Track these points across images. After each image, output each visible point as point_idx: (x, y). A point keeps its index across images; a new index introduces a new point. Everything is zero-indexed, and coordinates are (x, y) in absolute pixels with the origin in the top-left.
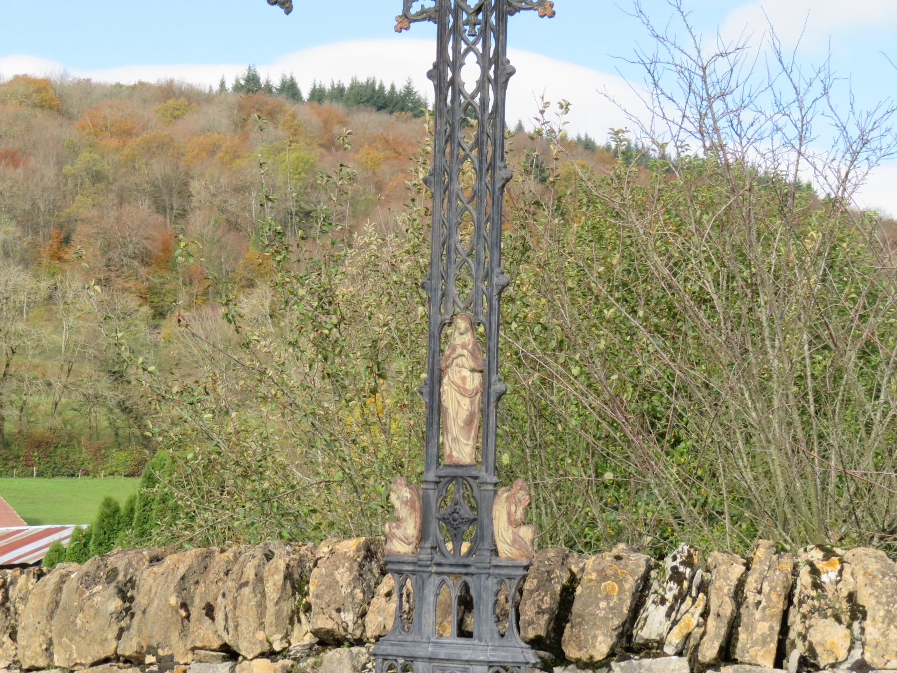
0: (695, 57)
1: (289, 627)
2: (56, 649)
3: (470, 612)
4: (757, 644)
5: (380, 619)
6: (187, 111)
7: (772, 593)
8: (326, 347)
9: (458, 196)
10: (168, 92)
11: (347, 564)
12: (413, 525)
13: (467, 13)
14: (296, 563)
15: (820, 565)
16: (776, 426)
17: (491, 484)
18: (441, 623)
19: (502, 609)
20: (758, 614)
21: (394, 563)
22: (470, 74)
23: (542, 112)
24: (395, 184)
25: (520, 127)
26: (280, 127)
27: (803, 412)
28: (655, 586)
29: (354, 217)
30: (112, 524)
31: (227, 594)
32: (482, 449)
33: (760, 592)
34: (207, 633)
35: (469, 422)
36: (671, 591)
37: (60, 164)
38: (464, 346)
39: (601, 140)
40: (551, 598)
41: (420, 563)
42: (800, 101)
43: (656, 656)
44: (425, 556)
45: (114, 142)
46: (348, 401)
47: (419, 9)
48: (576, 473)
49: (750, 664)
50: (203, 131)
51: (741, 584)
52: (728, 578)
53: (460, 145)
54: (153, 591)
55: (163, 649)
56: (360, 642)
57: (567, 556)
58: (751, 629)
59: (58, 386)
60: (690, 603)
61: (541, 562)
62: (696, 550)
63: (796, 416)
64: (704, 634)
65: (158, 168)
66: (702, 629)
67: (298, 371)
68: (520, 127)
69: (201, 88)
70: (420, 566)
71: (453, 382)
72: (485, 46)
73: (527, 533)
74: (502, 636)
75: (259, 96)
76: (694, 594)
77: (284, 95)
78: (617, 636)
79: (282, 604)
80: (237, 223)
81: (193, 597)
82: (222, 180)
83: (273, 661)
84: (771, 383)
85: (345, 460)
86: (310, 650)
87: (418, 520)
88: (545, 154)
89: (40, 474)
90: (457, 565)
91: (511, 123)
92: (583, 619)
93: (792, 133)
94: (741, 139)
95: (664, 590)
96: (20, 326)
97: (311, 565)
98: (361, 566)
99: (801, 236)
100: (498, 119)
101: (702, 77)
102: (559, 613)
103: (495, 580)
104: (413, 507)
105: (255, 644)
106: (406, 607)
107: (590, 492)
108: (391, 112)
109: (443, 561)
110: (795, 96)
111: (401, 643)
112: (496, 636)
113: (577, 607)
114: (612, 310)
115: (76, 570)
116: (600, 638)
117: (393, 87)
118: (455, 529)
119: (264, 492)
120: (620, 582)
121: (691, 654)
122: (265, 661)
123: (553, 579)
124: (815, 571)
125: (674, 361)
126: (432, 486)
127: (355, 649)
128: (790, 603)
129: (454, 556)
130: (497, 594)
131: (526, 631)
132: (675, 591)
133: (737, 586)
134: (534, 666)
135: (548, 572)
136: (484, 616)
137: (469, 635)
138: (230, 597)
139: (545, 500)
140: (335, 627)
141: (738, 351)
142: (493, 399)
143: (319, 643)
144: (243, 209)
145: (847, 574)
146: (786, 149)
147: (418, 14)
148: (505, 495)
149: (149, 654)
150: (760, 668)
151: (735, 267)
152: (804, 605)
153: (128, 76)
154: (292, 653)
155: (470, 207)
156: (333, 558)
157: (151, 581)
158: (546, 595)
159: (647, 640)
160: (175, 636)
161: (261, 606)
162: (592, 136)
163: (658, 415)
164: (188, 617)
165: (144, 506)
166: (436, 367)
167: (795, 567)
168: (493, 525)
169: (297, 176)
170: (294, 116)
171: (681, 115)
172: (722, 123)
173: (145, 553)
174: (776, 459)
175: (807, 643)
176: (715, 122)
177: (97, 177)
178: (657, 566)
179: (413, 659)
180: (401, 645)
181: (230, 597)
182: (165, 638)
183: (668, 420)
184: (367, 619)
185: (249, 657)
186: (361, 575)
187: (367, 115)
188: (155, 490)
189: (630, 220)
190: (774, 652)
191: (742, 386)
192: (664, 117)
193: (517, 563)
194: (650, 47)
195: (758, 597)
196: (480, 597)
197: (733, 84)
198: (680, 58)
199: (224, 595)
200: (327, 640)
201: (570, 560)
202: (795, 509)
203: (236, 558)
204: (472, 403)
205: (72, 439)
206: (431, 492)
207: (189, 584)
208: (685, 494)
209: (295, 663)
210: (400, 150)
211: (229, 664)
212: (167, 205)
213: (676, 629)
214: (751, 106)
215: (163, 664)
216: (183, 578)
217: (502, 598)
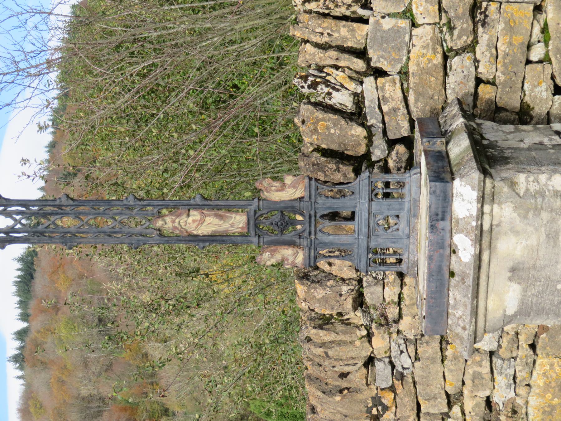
1: (352, 325)
3: (339, 213)
4: (354, 35)
5: (345, 269)
6: (37, 399)
7: (322, 26)
8: (181, 306)
9: (79, 228)
11: (312, 291)
12: (286, 250)
14: (312, 323)
16: (222, 25)
17: (259, 202)
18: (346, 231)
19: (337, 193)
20: (336, 35)
21: (310, 262)
23: (29, 177)
24: (80, 267)
25: (42, 189)
26: (45, 340)
27: (213, 8)
28: (320, 99)
29: (101, 292)
31: (333, 365)
33: (322, 34)
34: (358, 376)
35: (221, 217)
36: (322, 89)
38: (173, 222)
39: (47, 137)
40: (329, 163)
41: (309, 245)
42: (18, 14)
43: (363, 97)
44: (305, 242)
46: (214, 293)
48: (255, 149)
49: (367, 39)
51: (317, 45)
52: (314, 53)
54: (333, 411)
55: (368, 404)
56: (360, 281)
57: (303, 154)
58: (345, 39)
60: (330, 77)
61: (307, 170)
62: (297, 74)
63: (216, 13)
64: (349, 68)
66: (346, 69)
67: (195, 323)
68: (42, 189)
69: (22, 391)
70: (311, 245)
71: (196, 228)
73: (289, 179)
74: (353, 193)
75: (26, 353)
76: (324, 75)
77: (25, 339)
78: (351, 122)
79: (338, 330)
80: (107, 365)
81: (336, 386)
82: (80, 376)
83: (373, 335)
84: (196, 29)
85: (251, 293)
86: (366, 312)
87: (283, 247)
88: (60, 172)
90: (310, 222)
91: (37, 195)
92: (342, 143)
95: (322, 93)
97: (313, 313)
98: (313, 282)
100: (30, 204)
101: (4, 75)
102: (338, 158)
103: (319, 198)
104: (275, 251)
105: (363, 347)
106: (337, 253)
107: (267, 140)
108: (35, 270)
109: (308, 231)
110: (14, 17)
111: (359, 255)
112: (353, 197)
113: (334, 147)
114: (153, 130)
116: (353, 132)
117: (19, 270)
118: (288, 224)
119: (272, 342)
120: (318, 120)
121: (361, 76)
122: (374, 339)
123: (317, 162)
125: (184, 90)
126: (261, 239)
127: (365, 284)
128: (328, 15)
129: (304, 224)
130: (327, 197)
131: (350, 178)
132: (323, 86)
133: (319, 48)
134: (371, 173)
135: (313, 165)
136: (341, 205)
137: (353, 213)
138: (335, 363)
139: (273, 168)
140: (351, 297)
141: (176, 50)
142: (206, 203)
143: (361, 307)
144: (98, 362)
146: (49, 23)
148: (265, 193)
149: (371, 412)
150: (369, 33)
151: (124, 53)
152: (330, 6)
154: (368, 323)
155: (85, 220)
156: (309, 299)
157: (326, 412)
158: (328, 167)
159: (353, 103)
160: (360, 396)
161: (340, 343)
163: (218, 99)
164: (348, 389)
165: (285, 417)
166: (187, 239)
168: (284, 201)
169: (77, 329)
170: (38, 332)
171: (28, 88)
172: (33, 63)
173: (309, 417)
174: (244, 25)
175: (353, 4)
176: (32, 67)
178: (308, 98)
179: (369, 248)
180: (361, 256)
181: (335, 363)
182: (361, 402)
183: (221, 93)
184: (346, 277)
185: (371, 350)
186: (318, 282)
187: (36, 286)
188: (274, 411)
189: (96, 119)
190: (359, 24)
191: (198, 47)
192: (30, 99)
193: (307, 185)
195: (325, 35)
196: (329, 208)
197: (9, 56)
199: (334, 367)
200: (359, 302)
201: (306, 152)
203: (311, 360)
204: (209, 216)
206: (265, 240)
208: (266, 81)
209: (374, 321)
210: (58, 264)
211: (376, 362)
212: (97, 410)
213: (346, 85)
215: (377, 403)
216: (324, 393)
217: (330, 194)
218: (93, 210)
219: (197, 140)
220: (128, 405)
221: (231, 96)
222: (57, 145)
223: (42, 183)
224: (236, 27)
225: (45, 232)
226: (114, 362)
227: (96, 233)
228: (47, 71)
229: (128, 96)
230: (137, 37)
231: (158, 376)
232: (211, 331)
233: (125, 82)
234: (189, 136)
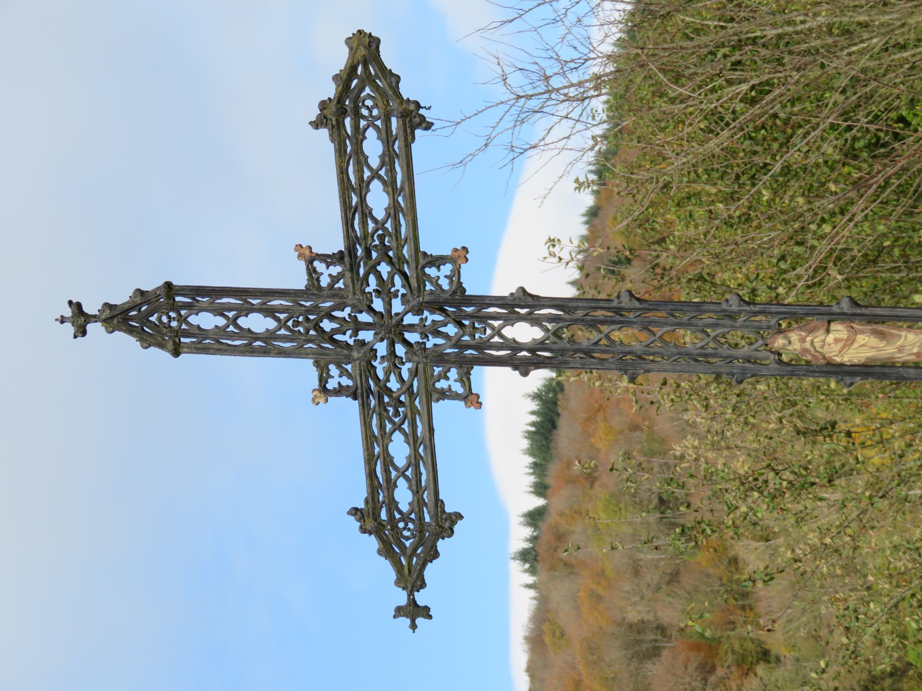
0: (506, 107)
6: (556, 623)
9: (648, 346)
10: (537, 641)
13: (462, 336)
25: (574, 283)
35: (882, 335)
38: (803, 340)
39: (587, 199)
46: (858, 462)
47: (459, 384)
53: (596, 344)
65: (615, 654)
67: (826, 508)
68: (574, 283)
69: (533, 608)
72: (496, 317)
75: (542, 549)
77: (540, 524)
80: (671, 574)
82: (627, 588)
88: (603, 257)
94: (590, 59)
108: (558, 415)
114: (764, 192)
117: (533, 413)
142: (858, 311)
144: (657, 568)
146: (601, 13)
147: (463, 385)
155: (659, 334)
162: (584, 210)
166: (824, 369)
169: (623, 512)
170: (562, 514)
171: (565, 120)
172: (574, 78)
176: (572, 85)
183: (881, 130)
194: (497, 152)
197: (534, 68)
204: (862, 332)
210: (596, 405)
212: (651, 645)
214: (556, 49)
218: (672, 318)
219: (837, 210)
220: (703, 641)
221: (896, 137)
222: (600, 212)
223: (576, 275)
224: (910, 21)
225: (593, 351)
226: (682, 570)
227: (675, 355)
228: (596, 93)
229: (726, 133)
230: (743, 37)
231: (754, 596)
232: (851, 525)
233: (720, 109)
234: (824, 201)
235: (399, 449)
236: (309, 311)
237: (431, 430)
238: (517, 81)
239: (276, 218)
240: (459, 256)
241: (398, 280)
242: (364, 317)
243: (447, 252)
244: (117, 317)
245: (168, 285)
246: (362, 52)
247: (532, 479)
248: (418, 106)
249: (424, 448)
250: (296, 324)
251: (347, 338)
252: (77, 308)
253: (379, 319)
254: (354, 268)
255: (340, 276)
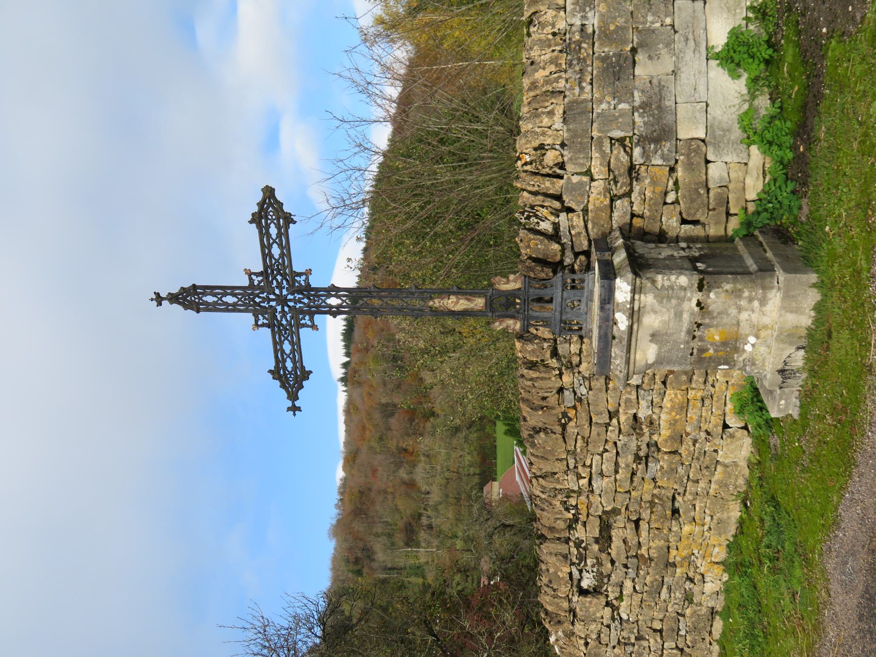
2: (560, 457)
10: (347, 412)
15: (523, 162)
20: (543, 186)
22: (333, 301)
27: (466, 167)
28: (532, 226)
30: (513, 432)
32: (479, 295)
34: (553, 400)
35: (469, 300)
36: (534, 220)
37: (376, 453)
39: (363, 245)
45: (367, 432)
50: (363, 399)
51: (530, 192)
56: (555, 340)
59: (462, 453)
65: (377, 415)
72: (323, 296)
73: (512, 277)
86: (559, 359)
89: (495, 459)
93: (358, 173)
96: (439, 468)
99: (398, 169)
106: (541, 323)
111: (555, 325)
113: (540, 256)
115: (530, 450)
120: (531, 240)
122: (563, 377)
124: (526, 164)
145: (527, 151)
153: (342, 428)
161: (542, 379)
167: (524, 171)
172: (354, 200)
177: (381, 439)
178: (524, 225)
179: (561, 321)
194: (325, 229)
198: (330, 217)
200: (555, 353)
202: (503, 170)
205: (482, 447)
207: (534, 406)
235: (287, 347)
236: (250, 294)
237: (299, 339)
238: (333, 202)
239: (239, 258)
240: (308, 273)
241: (284, 282)
242: (272, 297)
243: (303, 271)
244: (173, 298)
245: (194, 285)
246: (268, 194)
247: (344, 351)
248: (290, 214)
249: (297, 346)
250: (245, 299)
251: (265, 304)
252: (157, 294)
253: (279, 298)
254: (267, 278)
255: (262, 281)
